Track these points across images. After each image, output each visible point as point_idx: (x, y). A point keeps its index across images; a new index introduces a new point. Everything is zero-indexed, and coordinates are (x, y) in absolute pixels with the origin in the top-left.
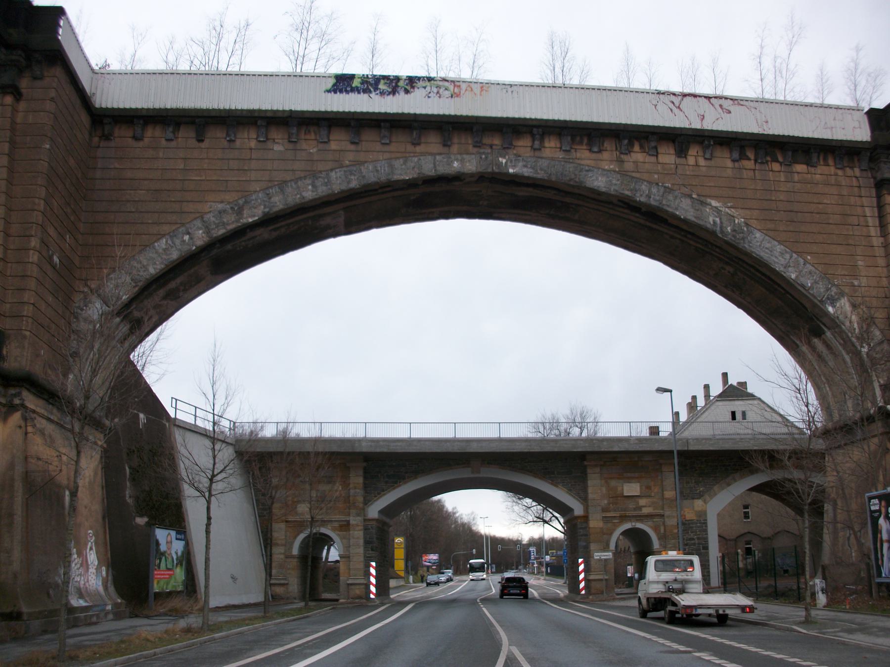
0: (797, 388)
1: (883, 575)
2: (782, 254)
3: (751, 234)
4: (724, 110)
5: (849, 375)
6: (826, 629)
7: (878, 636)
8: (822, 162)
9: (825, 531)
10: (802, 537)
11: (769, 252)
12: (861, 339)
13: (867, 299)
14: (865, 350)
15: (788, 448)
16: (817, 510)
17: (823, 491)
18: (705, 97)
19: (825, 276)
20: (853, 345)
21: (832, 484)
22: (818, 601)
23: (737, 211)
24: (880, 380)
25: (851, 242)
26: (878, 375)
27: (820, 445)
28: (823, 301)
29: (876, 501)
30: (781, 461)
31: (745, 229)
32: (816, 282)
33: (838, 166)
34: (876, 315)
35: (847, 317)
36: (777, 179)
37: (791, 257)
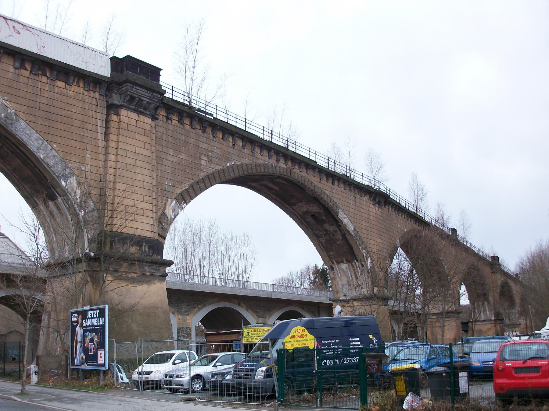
0: (32, 233)
1: (76, 364)
2: (37, 140)
3: (18, 122)
4: (16, 31)
5: (69, 229)
6: (34, 399)
7: (67, 403)
8: (75, 84)
9: (41, 332)
10: (23, 335)
11: (28, 137)
12: (80, 206)
13: (88, 180)
14: (82, 214)
15: (20, 273)
16: (37, 317)
17: (43, 306)
18: (4, 18)
19: (63, 160)
20: (75, 209)
21: (49, 301)
22: (31, 380)
23: (11, 104)
24: (89, 235)
25: (85, 141)
26: (88, 231)
27: (43, 274)
28: (59, 177)
29: (76, 315)
30: (15, 282)
31: (14, 117)
32: (57, 163)
33: (86, 89)
34: (92, 192)
35: (73, 190)
36: (43, 88)
37: (43, 143)
